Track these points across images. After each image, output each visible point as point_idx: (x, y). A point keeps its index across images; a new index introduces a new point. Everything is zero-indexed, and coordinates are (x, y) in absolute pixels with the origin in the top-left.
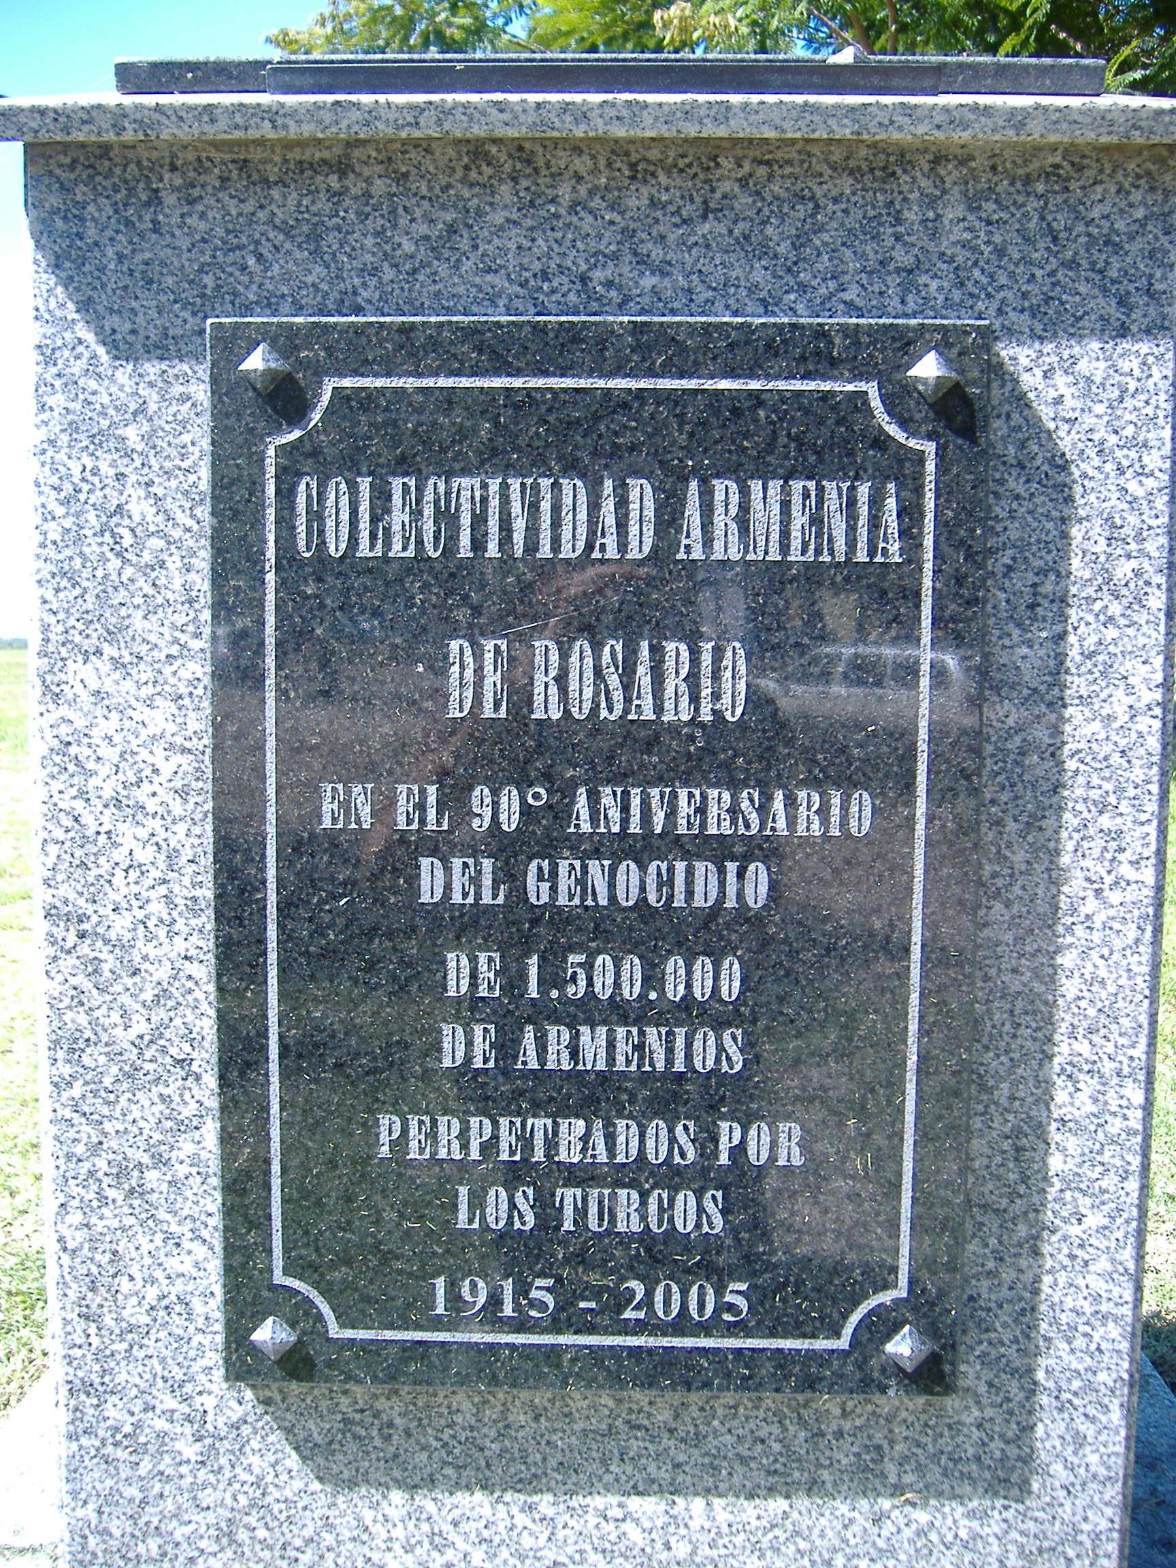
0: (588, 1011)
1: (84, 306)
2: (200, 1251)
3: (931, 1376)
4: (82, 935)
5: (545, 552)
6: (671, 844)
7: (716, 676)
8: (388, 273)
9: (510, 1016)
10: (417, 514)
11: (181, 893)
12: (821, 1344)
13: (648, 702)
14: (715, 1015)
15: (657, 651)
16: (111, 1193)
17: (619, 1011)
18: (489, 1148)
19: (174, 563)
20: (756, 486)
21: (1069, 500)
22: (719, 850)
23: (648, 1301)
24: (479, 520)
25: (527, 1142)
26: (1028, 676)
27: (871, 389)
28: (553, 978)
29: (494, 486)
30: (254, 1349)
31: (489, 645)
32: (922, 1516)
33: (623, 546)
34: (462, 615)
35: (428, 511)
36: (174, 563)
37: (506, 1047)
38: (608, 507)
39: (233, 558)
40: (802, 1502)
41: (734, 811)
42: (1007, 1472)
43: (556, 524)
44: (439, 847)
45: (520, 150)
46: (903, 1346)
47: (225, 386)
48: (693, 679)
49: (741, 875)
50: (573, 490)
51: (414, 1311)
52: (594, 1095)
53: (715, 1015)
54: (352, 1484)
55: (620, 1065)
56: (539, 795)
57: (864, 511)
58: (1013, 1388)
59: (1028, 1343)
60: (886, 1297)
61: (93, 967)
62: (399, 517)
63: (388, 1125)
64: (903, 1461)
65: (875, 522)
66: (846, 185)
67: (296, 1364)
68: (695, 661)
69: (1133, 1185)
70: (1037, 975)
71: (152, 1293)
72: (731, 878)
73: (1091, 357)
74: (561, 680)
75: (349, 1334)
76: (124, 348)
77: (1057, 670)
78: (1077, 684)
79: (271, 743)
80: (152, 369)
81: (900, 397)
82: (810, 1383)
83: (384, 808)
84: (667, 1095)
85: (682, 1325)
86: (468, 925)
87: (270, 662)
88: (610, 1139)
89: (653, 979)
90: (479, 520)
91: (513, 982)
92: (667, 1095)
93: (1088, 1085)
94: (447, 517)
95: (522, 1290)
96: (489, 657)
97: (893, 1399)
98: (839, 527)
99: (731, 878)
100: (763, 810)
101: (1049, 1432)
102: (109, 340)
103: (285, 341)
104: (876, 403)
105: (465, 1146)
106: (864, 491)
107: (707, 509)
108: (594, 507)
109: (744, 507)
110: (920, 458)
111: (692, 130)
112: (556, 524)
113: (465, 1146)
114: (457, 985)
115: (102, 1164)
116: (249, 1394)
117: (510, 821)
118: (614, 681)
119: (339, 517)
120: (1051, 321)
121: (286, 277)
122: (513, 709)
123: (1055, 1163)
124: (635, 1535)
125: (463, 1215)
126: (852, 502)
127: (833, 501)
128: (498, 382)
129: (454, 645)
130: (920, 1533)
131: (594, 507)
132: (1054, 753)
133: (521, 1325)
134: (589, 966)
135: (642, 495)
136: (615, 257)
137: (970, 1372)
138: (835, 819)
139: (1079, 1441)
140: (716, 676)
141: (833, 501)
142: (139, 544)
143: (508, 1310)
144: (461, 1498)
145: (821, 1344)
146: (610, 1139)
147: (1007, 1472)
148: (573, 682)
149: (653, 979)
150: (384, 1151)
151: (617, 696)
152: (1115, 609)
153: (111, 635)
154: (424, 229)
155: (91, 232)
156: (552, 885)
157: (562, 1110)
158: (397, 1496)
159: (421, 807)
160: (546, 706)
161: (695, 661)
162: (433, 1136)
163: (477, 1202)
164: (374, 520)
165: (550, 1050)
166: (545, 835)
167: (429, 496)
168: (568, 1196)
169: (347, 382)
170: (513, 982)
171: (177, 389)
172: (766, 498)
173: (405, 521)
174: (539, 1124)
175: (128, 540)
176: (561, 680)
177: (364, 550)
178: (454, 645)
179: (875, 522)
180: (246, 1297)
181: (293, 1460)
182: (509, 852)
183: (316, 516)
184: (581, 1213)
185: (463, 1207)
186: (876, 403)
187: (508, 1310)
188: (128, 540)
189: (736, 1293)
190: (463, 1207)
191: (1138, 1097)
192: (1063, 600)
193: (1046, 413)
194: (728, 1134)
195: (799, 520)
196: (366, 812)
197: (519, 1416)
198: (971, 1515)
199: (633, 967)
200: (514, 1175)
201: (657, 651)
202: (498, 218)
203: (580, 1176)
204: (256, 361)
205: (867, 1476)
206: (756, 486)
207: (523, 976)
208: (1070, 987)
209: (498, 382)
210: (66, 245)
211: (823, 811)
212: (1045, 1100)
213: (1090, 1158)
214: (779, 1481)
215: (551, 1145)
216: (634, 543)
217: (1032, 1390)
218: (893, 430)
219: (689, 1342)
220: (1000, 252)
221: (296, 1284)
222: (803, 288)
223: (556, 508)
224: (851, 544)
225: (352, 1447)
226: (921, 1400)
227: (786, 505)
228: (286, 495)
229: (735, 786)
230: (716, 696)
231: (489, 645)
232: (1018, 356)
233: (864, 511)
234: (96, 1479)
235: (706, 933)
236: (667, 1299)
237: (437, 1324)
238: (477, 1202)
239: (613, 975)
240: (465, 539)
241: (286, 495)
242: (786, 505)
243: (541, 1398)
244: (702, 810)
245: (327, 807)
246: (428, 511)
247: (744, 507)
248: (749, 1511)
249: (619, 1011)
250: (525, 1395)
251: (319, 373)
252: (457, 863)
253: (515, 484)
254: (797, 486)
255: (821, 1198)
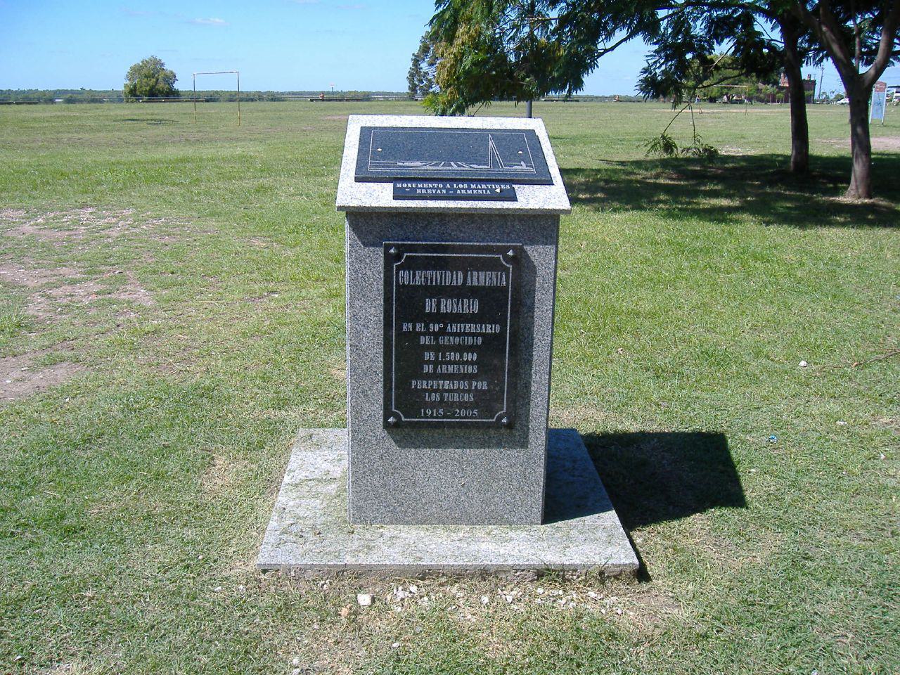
0: (450, 362)
1: (359, 237)
2: (378, 406)
3: (510, 426)
4: (357, 349)
5: (443, 284)
6: (465, 334)
7: (473, 305)
8: (415, 233)
9: (436, 363)
10: (421, 277)
11: (375, 341)
12: (490, 420)
13: (461, 310)
14: (472, 363)
15: (463, 301)
16: (361, 396)
17: (454, 363)
18: (432, 386)
19: (375, 283)
20: (480, 273)
21: (536, 273)
22: (473, 335)
23: (460, 413)
24: (432, 279)
25: (439, 386)
26: (528, 304)
27: (501, 256)
28: (444, 356)
29: (434, 273)
30: (389, 423)
31: (433, 300)
32: (509, 452)
33: (457, 283)
34: (429, 294)
35: (423, 277)
36: (375, 283)
37: (435, 369)
38: (455, 276)
39: (388, 283)
40: (487, 450)
41: (476, 328)
42: (524, 444)
43: (445, 279)
44: (424, 334)
45: (440, 214)
46: (504, 421)
47: (387, 255)
48: (469, 306)
49: (477, 339)
50: (448, 273)
51: (417, 415)
52: (450, 377)
53: (472, 363)
54: (405, 448)
55: (455, 372)
56: (442, 325)
57: (499, 277)
58: (525, 429)
59: (528, 421)
60: (502, 412)
61: (359, 355)
62: (417, 278)
63: (414, 383)
64: (505, 442)
65: (501, 279)
66: (498, 218)
67: (397, 425)
68: (469, 302)
69: (547, 393)
70: (529, 355)
71: (368, 414)
72: (475, 340)
73: (540, 248)
74: (446, 306)
75: (406, 420)
76: (365, 245)
77: (533, 303)
78: (537, 305)
79: (394, 316)
80: (371, 249)
81: (507, 258)
82: (489, 427)
83: (414, 328)
84: (464, 377)
85: (466, 417)
86: (428, 348)
87: (394, 302)
88: (453, 384)
89: (461, 357)
90: (432, 279)
91: (437, 357)
92: (464, 377)
93: (539, 375)
94: (426, 278)
95: (437, 411)
96: (433, 301)
97: (503, 431)
98: (495, 279)
99: (475, 340)
100: (481, 328)
101: (531, 437)
102: (363, 243)
103: (397, 247)
104: (501, 259)
105: (428, 386)
106: (499, 274)
107: (472, 277)
108: (452, 276)
109: (478, 276)
110: (509, 268)
111: (470, 212)
112: (445, 279)
113: (428, 386)
114: (426, 358)
115: (359, 390)
116: (386, 432)
117: (437, 330)
118: (455, 306)
119: (406, 277)
120: (533, 242)
121: (396, 233)
122: (437, 311)
123: (532, 388)
124: (456, 456)
125: (427, 398)
126: (497, 276)
127: (494, 276)
128: (435, 255)
129: (427, 300)
130: (508, 455)
131: (452, 276)
132: (533, 317)
133: (437, 417)
134: (450, 355)
135: (460, 274)
136: (456, 231)
137: (518, 426)
138: (493, 329)
139: (537, 438)
140: (473, 305)
141: (494, 276)
142: (369, 280)
143: (435, 415)
144: (425, 450)
145: (490, 420)
146: (453, 384)
147: (524, 444)
148: (447, 306)
149: (461, 357)
150: (413, 387)
151: (456, 308)
152: (544, 292)
153: (363, 296)
154: (421, 225)
155: (360, 224)
156: (444, 341)
157: (444, 379)
158: (413, 450)
159: (421, 327)
160: (443, 310)
161: (469, 302)
162: (422, 384)
163: (430, 396)
164: (413, 278)
165: (443, 369)
166: (443, 332)
167: (423, 274)
168: (446, 394)
169: (408, 254)
170: (437, 357)
171: (376, 253)
172: (482, 275)
173: (420, 278)
174: (441, 382)
175: (367, 279)
176: (446, 306)
177: (411, 283)
178: (427, 300)
179: (501, 279)
180: (387, 413)
181: (394, 444)
182: (436, 335)
183: (403, 278)
184: (448, 397)
185: (427, 396)
186: (501, 259)
187: (435, 415)
188: (367, 279)
189: (475, 411)
190: (427, 396)
191: (547, 377)
192: (534, 290)
193: (532, 258)
194: (474, 384)
195: (487, 279)
196: (411, 328)
197: (436, 435)
198: (517, 452)
199: (458, 355)
200: (436, 391)
201: (463, 301)
202: (435, 223)
203: (448, 391)
204: (392, 251)
205: (499, 445)
206: (480, 273)
207: (438, 357)
208: (535, 358)
209: (435, 255)
210: (355, 227)
211: (491, 328)
212: (531, 377)
213: (538, 388)
214: (483, 446)
215: (443, 386)
216: (459, 283)
217: (528, 429)
218: (504, 263)
219: (467, 420)
220: (525, 230)
221: (397, 411)
222: (489, 236)
223: (445, 276)
224: (497, 283)
225: (405, 441)
226: (508, 431)
227: (485, 276)
228: (397, 274)
229: (476, 324)
230: (473, 309)
231: (433, 300)
232: (527, 248)
233: (499, 277)
234: (356, 448)
235: (471, 348)
236: (463, 413)
237: (422, 417)
238: (430, 396)
239: (452, 356)
240: (429, 281)
241: (397, 274)
242: (485, 276)
243: (440, 431)
244: (470, 328)
245: (404, 327)
246: (423, 277)
247: (478, 276)
248: (478, 451)
249: (454, 363)
250: (437, 431)
251: (403, 252)
252: (427, 337)
253: (438, 273)
254: (487, 273)
255: (739, 441)
